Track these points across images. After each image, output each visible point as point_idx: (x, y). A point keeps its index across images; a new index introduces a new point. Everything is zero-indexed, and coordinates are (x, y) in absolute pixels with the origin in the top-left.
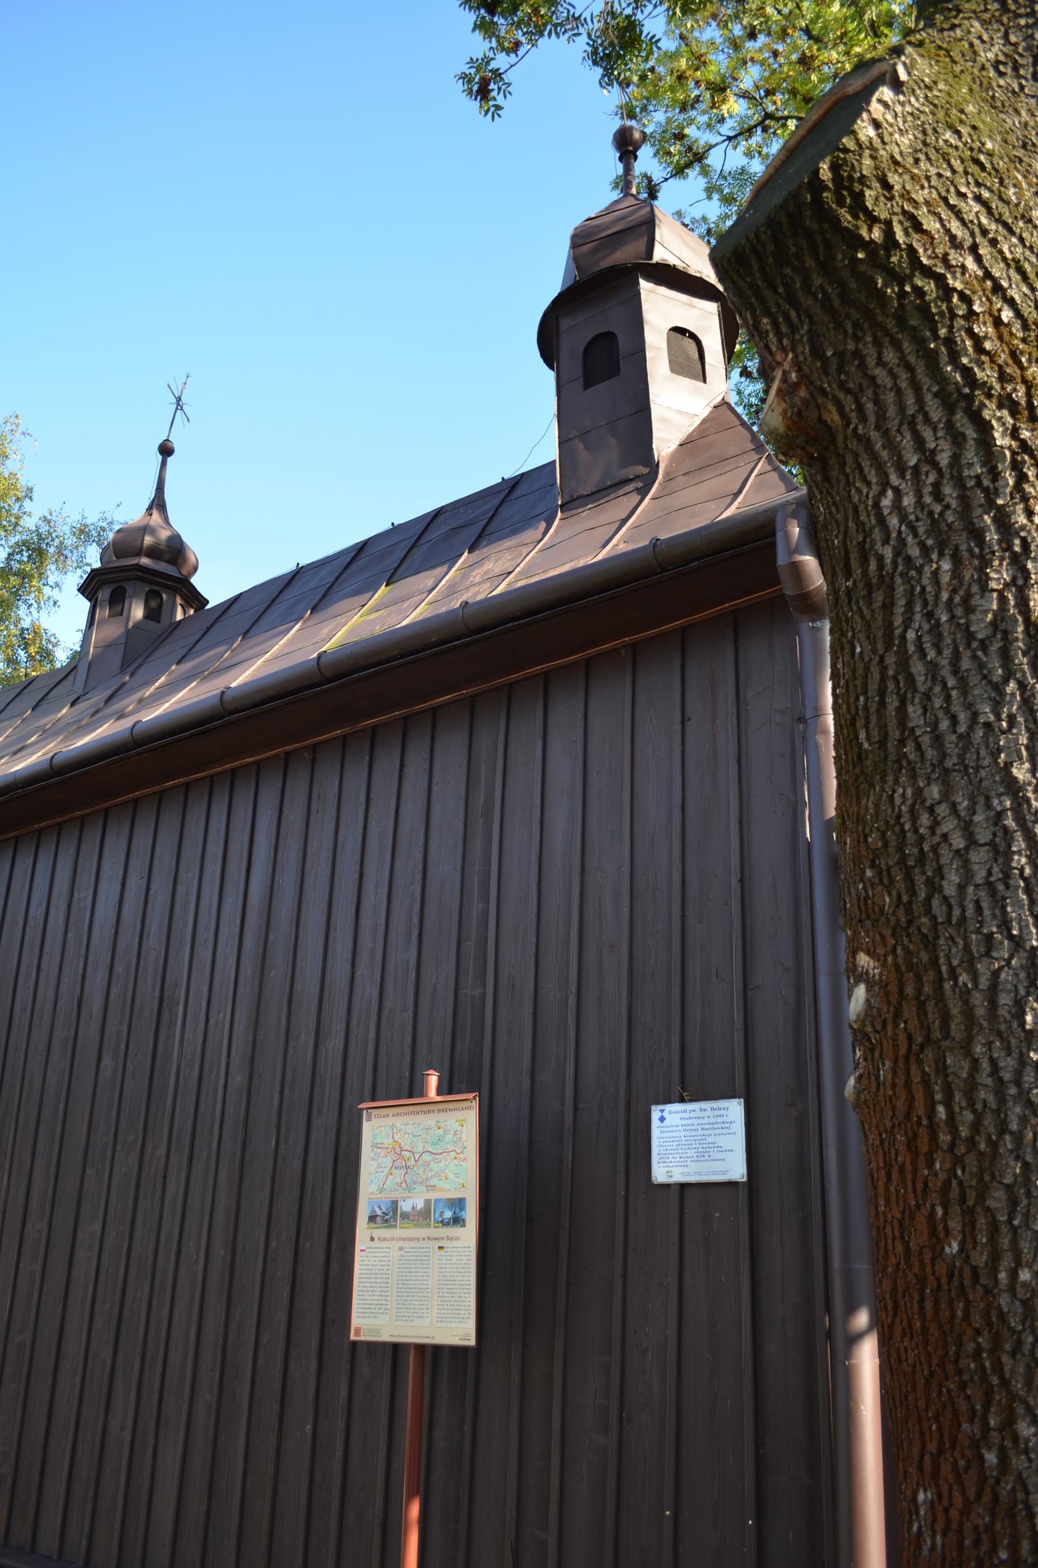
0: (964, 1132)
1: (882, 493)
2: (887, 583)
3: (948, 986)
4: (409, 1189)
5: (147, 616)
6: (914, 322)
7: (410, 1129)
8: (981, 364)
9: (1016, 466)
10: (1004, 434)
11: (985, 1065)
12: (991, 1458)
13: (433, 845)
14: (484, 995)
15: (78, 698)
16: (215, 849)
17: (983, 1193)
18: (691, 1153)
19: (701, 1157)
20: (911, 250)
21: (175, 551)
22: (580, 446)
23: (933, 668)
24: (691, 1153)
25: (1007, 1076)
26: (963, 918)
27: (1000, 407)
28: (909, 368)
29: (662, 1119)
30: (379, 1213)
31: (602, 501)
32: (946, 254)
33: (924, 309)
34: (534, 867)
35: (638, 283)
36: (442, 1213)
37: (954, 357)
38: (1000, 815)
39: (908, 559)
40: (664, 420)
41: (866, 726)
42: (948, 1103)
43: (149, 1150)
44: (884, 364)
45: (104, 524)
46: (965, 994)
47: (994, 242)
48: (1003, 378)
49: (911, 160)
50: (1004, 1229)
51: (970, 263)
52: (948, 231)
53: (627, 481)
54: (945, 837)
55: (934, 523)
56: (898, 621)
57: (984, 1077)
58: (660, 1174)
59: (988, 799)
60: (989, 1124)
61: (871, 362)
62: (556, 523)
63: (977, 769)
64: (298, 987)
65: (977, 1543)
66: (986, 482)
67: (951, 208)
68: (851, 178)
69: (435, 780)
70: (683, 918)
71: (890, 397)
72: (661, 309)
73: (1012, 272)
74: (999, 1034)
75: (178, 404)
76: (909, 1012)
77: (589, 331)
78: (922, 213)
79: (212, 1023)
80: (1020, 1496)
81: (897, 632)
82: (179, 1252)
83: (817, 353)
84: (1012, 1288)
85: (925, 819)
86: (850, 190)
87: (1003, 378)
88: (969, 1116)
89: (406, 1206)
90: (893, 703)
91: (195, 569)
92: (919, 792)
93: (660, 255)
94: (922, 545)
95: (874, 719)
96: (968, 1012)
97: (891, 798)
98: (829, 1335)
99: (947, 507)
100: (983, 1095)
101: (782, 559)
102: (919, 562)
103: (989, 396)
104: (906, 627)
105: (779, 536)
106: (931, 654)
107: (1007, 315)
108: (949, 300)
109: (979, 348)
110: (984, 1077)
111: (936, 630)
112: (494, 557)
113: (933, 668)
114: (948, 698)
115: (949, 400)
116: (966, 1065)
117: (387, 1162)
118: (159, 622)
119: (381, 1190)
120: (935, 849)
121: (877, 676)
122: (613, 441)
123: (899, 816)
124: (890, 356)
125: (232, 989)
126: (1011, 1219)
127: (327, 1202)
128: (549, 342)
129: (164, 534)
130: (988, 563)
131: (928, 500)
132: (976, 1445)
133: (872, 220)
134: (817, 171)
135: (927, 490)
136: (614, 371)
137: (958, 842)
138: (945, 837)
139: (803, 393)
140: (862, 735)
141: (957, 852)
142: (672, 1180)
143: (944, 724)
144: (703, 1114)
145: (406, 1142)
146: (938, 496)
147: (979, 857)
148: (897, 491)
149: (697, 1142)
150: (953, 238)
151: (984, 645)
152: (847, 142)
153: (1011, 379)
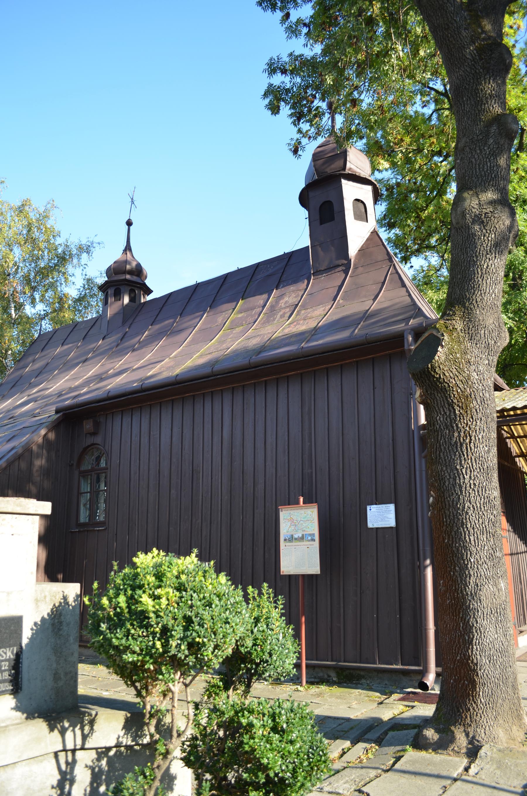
2: (438, 431)
4: (297, 531)
5: (130, 301)
9: (459, 416)
13: (291, 423)
14: (312, 472)
16: (208, 419)
17: (451, 532)
21: (139, 271)
22: (320, 249)
23: (445, 448)
34: (327, 432)
37: (450, 397)
43: (194, 520)
44: (438, 396)
46: (449, 501)
51: (454, 382)
55: (446, 424)
57: (451, 514)
58: (370, 525)
64: (245, 468)
69: (290, 401)
70: (375, 451)
72: (351, 191)
75: (132, 199)
76: (440, 503)
78: (446, 373)
79: (213, 479)
82: (209, 553)
83: (427, 391)
89: (296, 536)
90: (438, 452)
91: (146, 277)
96: (449, 504)
98: (419, 567)
101: (406, 347)
105: (405, 340)
107: (459, 391)
110: (451, 514)
111: (445, 441)
113: (445, 448)
115: (449, 405)
117: (289, 524)
122: (332, 248)
124: (439, 395)
127: (263, 536)
128: (304, 199)
129: (134, 264)
132: (450, 572)
133: (437, 374)
136: (332, 219)
137: (448, 477)
147: (451, 480)
149: (381, 516)
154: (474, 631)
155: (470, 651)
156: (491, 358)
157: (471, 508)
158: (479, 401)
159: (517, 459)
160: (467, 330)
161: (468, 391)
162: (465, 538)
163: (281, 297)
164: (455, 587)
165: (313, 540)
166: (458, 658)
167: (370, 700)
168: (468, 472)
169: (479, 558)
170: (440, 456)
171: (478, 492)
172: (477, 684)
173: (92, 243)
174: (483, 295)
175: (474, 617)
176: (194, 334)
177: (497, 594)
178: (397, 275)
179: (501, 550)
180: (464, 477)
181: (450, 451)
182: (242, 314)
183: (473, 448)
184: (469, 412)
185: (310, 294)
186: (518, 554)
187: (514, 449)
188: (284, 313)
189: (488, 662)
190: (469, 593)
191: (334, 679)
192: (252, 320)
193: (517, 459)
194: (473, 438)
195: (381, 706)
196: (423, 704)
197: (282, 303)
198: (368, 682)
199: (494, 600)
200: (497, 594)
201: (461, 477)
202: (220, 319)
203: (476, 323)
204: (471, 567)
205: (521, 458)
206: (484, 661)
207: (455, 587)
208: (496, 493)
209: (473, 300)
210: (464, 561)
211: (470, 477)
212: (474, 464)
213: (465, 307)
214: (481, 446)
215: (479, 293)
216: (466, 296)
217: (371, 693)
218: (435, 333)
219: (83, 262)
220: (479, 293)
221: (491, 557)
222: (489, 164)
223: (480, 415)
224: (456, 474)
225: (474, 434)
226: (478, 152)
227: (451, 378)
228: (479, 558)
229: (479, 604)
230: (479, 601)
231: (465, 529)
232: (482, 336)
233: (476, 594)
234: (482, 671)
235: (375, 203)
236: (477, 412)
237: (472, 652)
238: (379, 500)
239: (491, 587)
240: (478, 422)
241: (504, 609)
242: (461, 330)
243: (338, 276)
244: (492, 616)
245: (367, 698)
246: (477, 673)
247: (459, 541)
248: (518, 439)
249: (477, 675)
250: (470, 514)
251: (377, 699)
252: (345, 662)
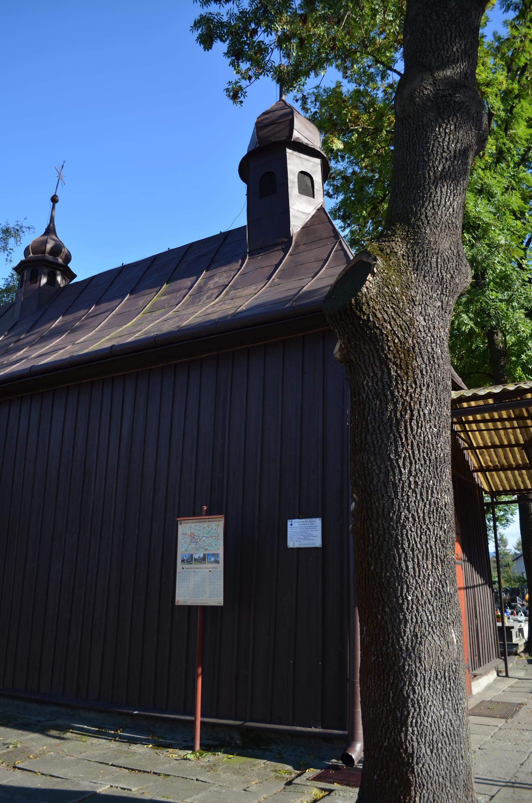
0: (376, 541)
1: (364, 380)
3: (373, 506)
4: (197, 550)
6: (373, 340)
7: (197, 528)
8: (389, 354)
9: (396, 380)
10: (393, 372)
11: (381, 525)
12: (379, 617)
15: (17, 323)
18: (302, 537)
19: (305, 538)
20: (374, 322)
21: (58, 249)
23: (374, 428)
24: (302, 537)
25: (386, 528)
26: (377, 490)
27: (393, 365)
28: (372, 351)
29: (291, 525)
30: (185, 559)
31: (267, 252)
32: (383, 324)
33: (376, 337)
35: (286, 150)
36: (210, 559)
37: (383, 350)
38: (387, 466)
39: (369, 399)
40: (295, 216)
41: (358, 438)
42: (372, 534)
45: (18, 228)
47: (395, 320)
48: (395, 357)
49: (375, 296)
50: (384, 564)
51: (389, 327)
52: (383, 317)
53: (278, 244)
54: (374, 470)
56: (366, 414)
57: (381, 528)
59: (385, 462)
60: (381, 538)
61: (363, 348)
62: (246, 261)
63: (383, 454)
65: (376, 637)
66: (389, 383)
67: (385, 311)
68: (360, 303)
71: (367, 357)
72: (296, 163)
73: (399, 328)
74: (384, 518)
75: (60, 174)
77: (263, 169)
78: (377, 313)
80: (386, 625)
81: (366, 416)
83: (349, 342)
84: (385, 577)
85: (370, 465)
86: (359, 306)
87: (394, 357)
88: (377, 537)
89: (196, 556)
90: (364, 435)
92: (369, 458)
93: (296, 134)
94: (373, 396)
95: (359, 437)
96: (378, 512)
97: (362, 458)
99: (379, 388)
100: (380, 532)
102: (372, 400)
103: (391, 362)
104: (368, 416)
106: (373, 424)
107: (396, 341)
108: (383, 336)
109: (389, 349)
110: (381, 528)
112: (218, 275)
113: (374, 428)
114: (377, 436)
116: (377, 525)
118: (54, 286)
119: (186, 550)
120: (372, 472)
121: (361, 426)
123: (364, 463)
124: (367, 347)
125: (116, 470)
126: (385, 561)
128: (245, 170)
130: (388, 404)
131: (375, 385)
133: (364, 314)
134: (351, 301)
135: (375, 383)
137: (377, 471)
138: (374, 470)
139: (345, 351)
140: (356, 440)
141: (377, 474)
142: (295, 547)
143: (376, 442)
144: (306, 523)
145: (196, 533)
146: (377, 385)
148: (367, 381)
149: (304, 533)
150: (385, 319)
151: (386, 424)
152: (359, 294)
153: (396, 358)
154: (410, 705)
155: (403, 735)
156: (445, 299)
157: (411, 519)
158: (426, 358)
159: (475, 474)
160: (410, 255)
161: (410, 342)
162: (400, 563)
163: (211, 278)
164: (384, 638)
165: (217, 562)
166: (386, 744)
167: (277, 777)
168: (407, 464)
169: (419, 595)
170: (366, 440)
171: (421, 494)
172: (412, 785)
173: (21, 227)
174: (436, 208)
175: (410, 684)
176: (111, 318)
177: (445, 649)
178: (342, 252)
179: (453, 582)
180: (400, 472)
181: (380, 432)
182: (166, 297)
183: (415, 428)
184: (410, 374)
185: (242, 274)
186: (474, 587)
187: (473, 462)
188: (212, 294)
189: (429, 753)
190: (404, 648)
191: (238, 742)
192: (174, 302)
193: (475, 474)
194: (415, 413)
195: (289, 788)
196: (345, 787)
197: (211, 284)
198: (280, 748)
199: (441, 658)
200: (445, 649)
201: (397, 471)
202: (141, 303)
203: (425, 246)
204: (408, 609)
205: (479, 474)
206: (423, 751)
207: (384, 638)
208: (448, 498)
209: (421, 214)
210: (397, 598)
211: (410, 472)
212: (416, 452)
213: (409, 225)
214: (428, 427)
215: (431, 205)
216: (412, 209)
217: (280, 766)
218: (365, 259)
219: (10, 246)
220: (431, 205)
221: (438, 594)
222: (449, 34)
223: (426, 379)
224: (391, 467)
225: (417, 407)
226: (435, 18)
227: (385, 321)
228: (419, 595)
229: (418, 665)
230: (418, 660)
231: (401, 551)
232: (434, 265)
233: (413, 649)
234: (420, 765)
235: (324, 181)
236: (422, 374)
237: (406, 736)
238: (303, 513)
239: (436, 639)
240: (424, 389)
241: (455, 672)
242: (403, 255)
243: (276, 256)
244: (437, 682)
245: (272, 774)
246: (413, 769)
247: (391, 568)
248: (477, 451)
249: (413, 772)
250: (408, 528)
251: (286, 776)
252: (251, 721)
